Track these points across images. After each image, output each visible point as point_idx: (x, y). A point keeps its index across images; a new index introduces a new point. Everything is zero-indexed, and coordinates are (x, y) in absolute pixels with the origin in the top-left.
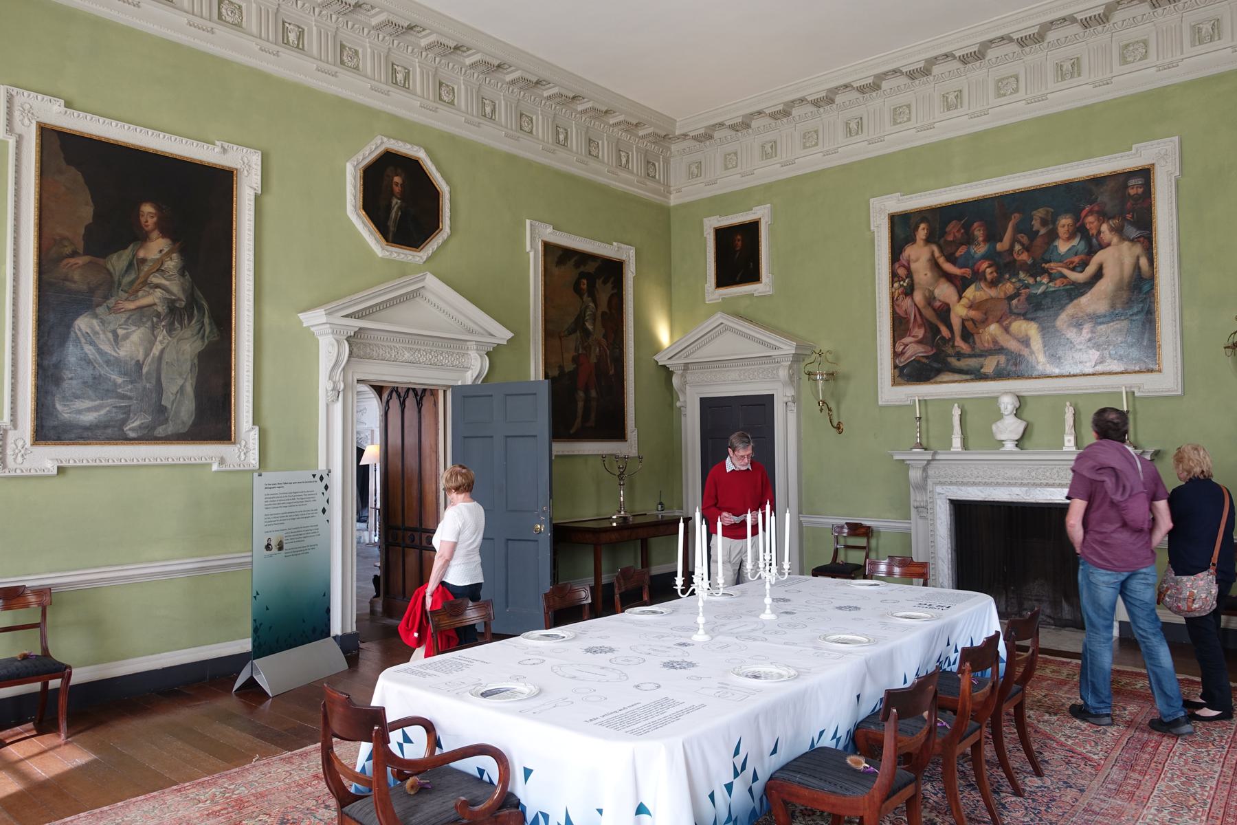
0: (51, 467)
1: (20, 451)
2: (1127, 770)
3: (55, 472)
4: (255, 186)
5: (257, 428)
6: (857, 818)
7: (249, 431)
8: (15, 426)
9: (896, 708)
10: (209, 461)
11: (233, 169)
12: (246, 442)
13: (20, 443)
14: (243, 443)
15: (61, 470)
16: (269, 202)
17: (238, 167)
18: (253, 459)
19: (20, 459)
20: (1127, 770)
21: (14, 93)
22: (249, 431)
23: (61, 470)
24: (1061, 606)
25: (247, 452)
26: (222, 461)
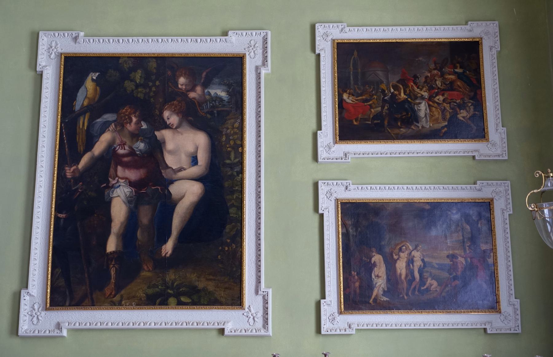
0: (233, 37)
1: (252, 49)
2: (137, 86)
3: (230, 33)
4: (27, 298)
5: (38, 69)
6: (380, 90)
7: (46, 66)
8: (257, 68)
9: (176, 83)
10: (87, 39)
11: (51, 310)
12: (50, 57)
13: (252, 54)
14: (53, 56)
15: (225, 34)
16: (13, 284)
17: (43, 313)
18: (44, 41)
19: (253, 43)
20: (137, 86)
21: (56, 331)
22: (46, 66)
23: (225, 34)
24: (487, 260)
25: (49, 49)
26: (76, 39)
